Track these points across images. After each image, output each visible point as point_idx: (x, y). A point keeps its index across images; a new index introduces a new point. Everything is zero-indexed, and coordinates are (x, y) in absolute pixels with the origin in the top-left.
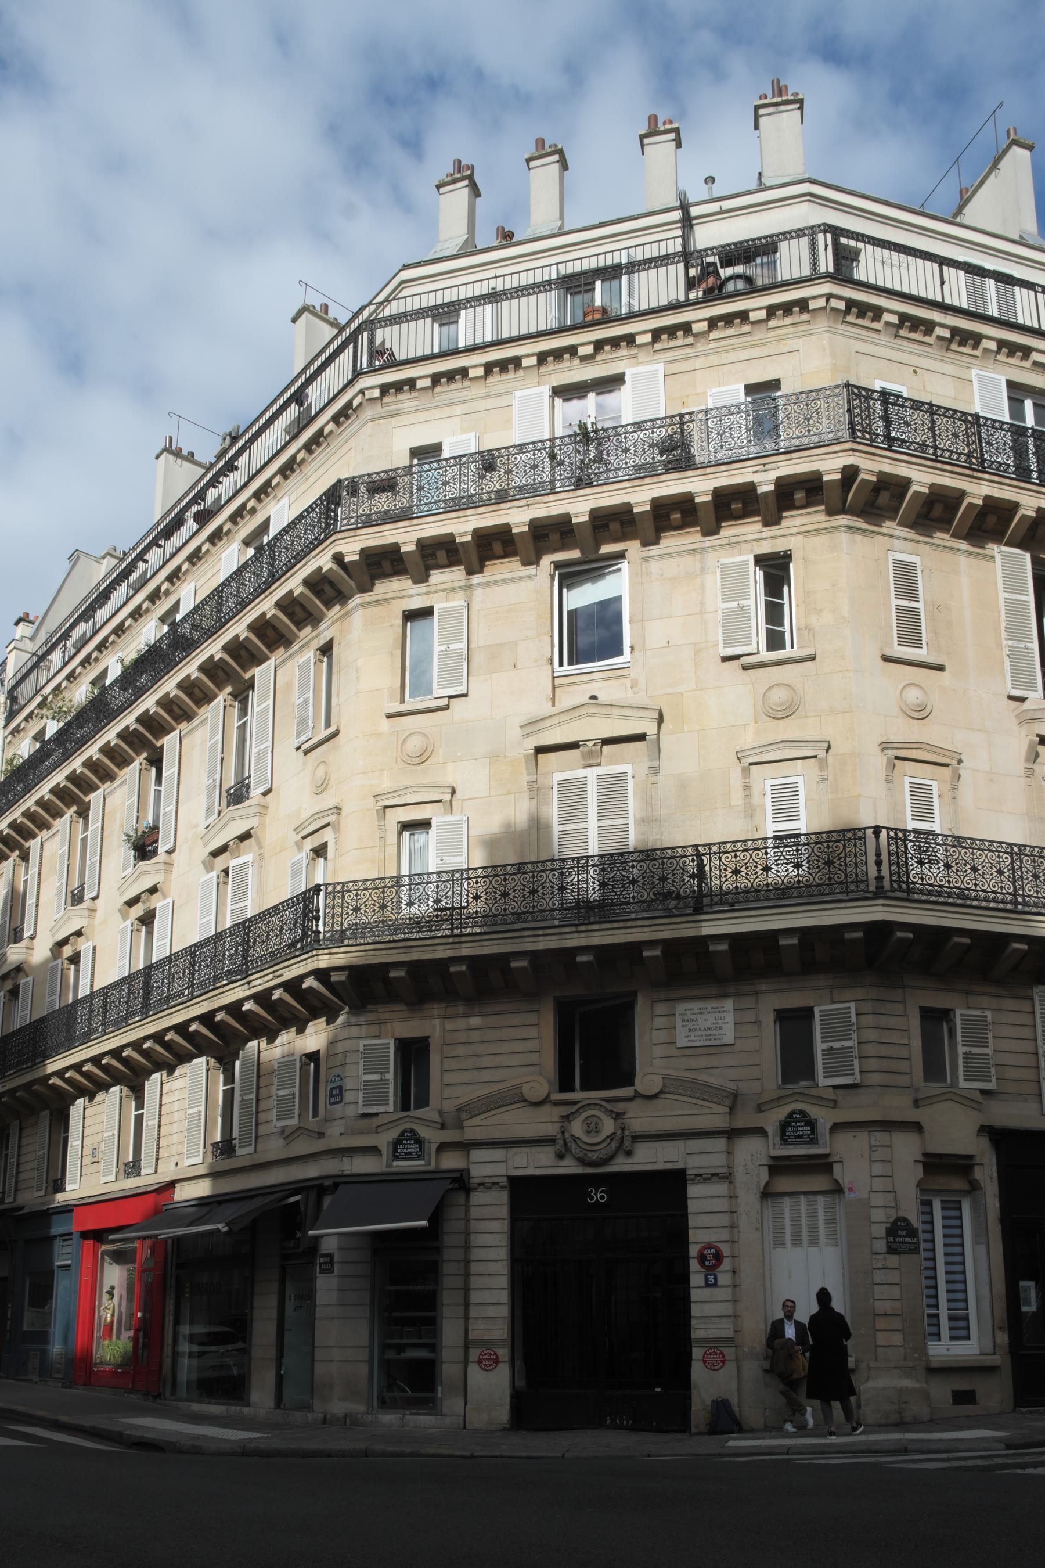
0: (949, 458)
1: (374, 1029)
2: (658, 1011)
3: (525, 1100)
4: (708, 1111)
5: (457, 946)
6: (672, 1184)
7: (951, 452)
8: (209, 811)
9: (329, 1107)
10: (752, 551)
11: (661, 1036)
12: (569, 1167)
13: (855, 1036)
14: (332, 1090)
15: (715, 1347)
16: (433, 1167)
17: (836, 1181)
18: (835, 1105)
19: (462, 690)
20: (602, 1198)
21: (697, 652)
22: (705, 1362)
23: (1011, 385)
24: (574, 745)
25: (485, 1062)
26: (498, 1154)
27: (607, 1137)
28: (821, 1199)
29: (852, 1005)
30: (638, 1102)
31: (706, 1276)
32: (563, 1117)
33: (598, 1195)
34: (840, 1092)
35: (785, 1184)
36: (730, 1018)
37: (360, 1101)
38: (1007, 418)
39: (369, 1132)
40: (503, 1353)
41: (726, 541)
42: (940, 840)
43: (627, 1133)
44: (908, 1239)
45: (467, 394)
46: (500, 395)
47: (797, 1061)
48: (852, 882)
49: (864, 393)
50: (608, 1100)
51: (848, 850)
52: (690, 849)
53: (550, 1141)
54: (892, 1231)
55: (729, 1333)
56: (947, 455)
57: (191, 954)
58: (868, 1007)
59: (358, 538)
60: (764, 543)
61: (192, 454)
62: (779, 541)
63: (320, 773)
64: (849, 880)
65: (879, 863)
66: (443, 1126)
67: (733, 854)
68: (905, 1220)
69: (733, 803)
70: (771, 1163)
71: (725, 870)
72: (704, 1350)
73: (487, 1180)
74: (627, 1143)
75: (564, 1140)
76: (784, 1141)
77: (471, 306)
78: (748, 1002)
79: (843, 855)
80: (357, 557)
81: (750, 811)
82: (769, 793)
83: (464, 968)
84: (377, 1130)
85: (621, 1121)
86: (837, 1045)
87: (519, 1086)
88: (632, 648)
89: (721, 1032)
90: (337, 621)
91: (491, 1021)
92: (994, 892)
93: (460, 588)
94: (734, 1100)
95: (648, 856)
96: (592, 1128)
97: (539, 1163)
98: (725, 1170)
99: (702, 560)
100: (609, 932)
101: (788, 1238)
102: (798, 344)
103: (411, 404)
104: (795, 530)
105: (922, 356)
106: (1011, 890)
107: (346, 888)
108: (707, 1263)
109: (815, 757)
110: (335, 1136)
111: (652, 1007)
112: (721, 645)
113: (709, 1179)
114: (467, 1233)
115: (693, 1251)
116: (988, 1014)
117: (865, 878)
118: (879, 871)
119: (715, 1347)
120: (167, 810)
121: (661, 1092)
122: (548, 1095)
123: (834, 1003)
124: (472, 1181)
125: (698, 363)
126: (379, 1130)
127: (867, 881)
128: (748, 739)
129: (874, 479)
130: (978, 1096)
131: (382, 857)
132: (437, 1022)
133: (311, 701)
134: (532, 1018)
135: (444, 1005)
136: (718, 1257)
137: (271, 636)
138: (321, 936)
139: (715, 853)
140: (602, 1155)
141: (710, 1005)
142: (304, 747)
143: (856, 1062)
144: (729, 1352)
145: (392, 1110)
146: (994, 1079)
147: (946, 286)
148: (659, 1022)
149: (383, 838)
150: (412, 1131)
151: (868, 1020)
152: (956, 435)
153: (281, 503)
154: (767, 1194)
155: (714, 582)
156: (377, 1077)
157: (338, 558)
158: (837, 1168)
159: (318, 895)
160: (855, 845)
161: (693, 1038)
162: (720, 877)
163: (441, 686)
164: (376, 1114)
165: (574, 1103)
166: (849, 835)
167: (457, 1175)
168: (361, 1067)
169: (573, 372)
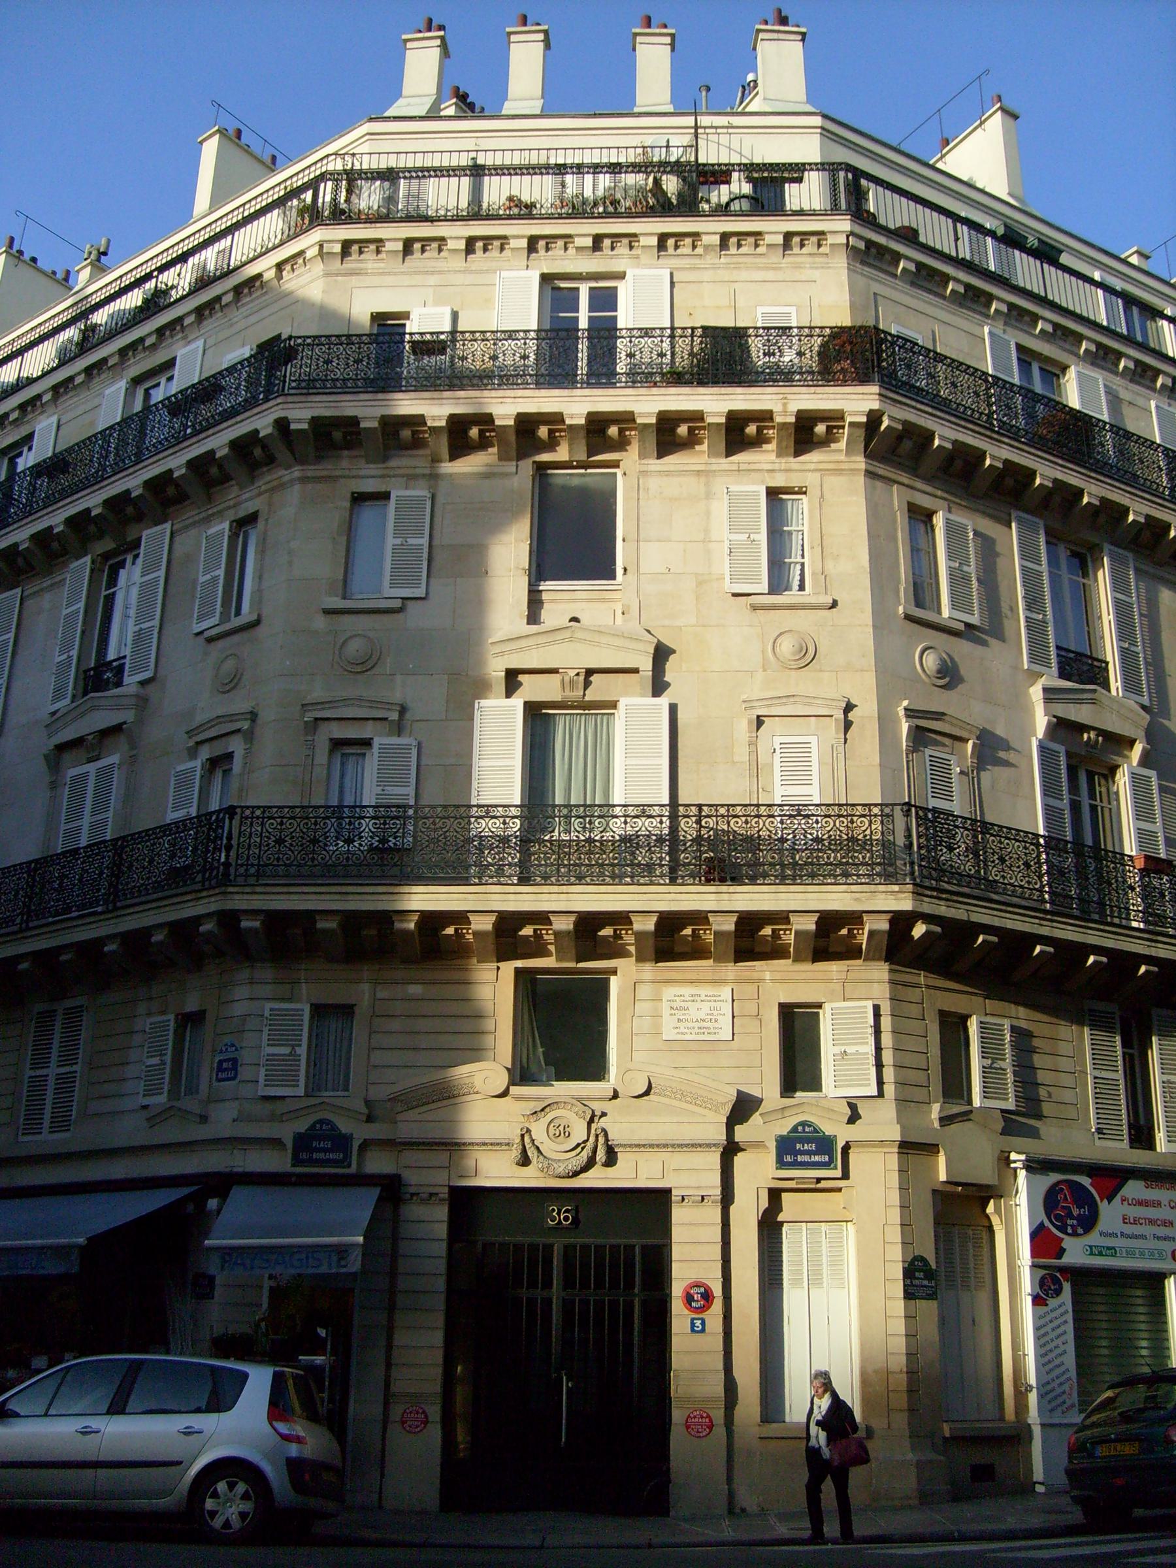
0: (963, 413)
7: (973, 411)
8: (58, 694)
10: (763, 482)
16: (353, 1169)
19: (420, 592)
20: (566, 1219)
21: (700, 584)
22: (688, 1427)
23: (1020, 348)
24: (554, 671)
27: (578, 1145)
31: (693, 1320)
38: (1016, 381)
39: (272, 1118)
41: (735, 467)
42: (959, 822)
44: (926, 1283)
45: (441, 265)
46: (481, 272)
49: (889, 338)
51: (873, 827)
52: (693, 808)
54: (908, 1273)
56: (969, 413)
57: (28, 872)
59: (309, 405)
60: (778, 475)
61: (34, 260)
62: (793, 475)
63: (230, 665)
66: (370, 1119)
68: (922, 1259)
73: (422, 1190)
77: (456, 175)
79: (868, 832)
80: (305, 426)
81: (756, 769)
84: (281, 1118)
88: (625, 570)
89: (716, 1025)
90: (266, 491)
92: (1021, 887)
93: (424, 475)
95: (644, 811)
99: (707, 484)
102: (816, 274)
103: (376, 265)
104: (812, 466)
105: (935, 306)
106: (1037, 887)
107: (267, 814)
108: (694, 1304)
110: (224, 1120)
112: (727, 580)
115: (677, 1290)
124: (403, 1189)
125: (707, 276)
128: (756, 689)
129: (900, 427)
132: (366, 987)
133: (221, 581)
135: (377, 967)
136: (707, 1296)
137: (165, 497)
138: (232, 870)
139: (723, 816)
142: (207, 634)
145: (301, 1091)
147: (960, 243)
150: (329, 1122)
152: (977, 394)
153: (193, 346)
155: (720, 508)
156: (286, 1050)
157: (282, 425)
159: (231, 819)
161: (682, 1030)
163: (393, 585)
164: (283, 1098)
168: (265, 1037)
169: (566, 262)
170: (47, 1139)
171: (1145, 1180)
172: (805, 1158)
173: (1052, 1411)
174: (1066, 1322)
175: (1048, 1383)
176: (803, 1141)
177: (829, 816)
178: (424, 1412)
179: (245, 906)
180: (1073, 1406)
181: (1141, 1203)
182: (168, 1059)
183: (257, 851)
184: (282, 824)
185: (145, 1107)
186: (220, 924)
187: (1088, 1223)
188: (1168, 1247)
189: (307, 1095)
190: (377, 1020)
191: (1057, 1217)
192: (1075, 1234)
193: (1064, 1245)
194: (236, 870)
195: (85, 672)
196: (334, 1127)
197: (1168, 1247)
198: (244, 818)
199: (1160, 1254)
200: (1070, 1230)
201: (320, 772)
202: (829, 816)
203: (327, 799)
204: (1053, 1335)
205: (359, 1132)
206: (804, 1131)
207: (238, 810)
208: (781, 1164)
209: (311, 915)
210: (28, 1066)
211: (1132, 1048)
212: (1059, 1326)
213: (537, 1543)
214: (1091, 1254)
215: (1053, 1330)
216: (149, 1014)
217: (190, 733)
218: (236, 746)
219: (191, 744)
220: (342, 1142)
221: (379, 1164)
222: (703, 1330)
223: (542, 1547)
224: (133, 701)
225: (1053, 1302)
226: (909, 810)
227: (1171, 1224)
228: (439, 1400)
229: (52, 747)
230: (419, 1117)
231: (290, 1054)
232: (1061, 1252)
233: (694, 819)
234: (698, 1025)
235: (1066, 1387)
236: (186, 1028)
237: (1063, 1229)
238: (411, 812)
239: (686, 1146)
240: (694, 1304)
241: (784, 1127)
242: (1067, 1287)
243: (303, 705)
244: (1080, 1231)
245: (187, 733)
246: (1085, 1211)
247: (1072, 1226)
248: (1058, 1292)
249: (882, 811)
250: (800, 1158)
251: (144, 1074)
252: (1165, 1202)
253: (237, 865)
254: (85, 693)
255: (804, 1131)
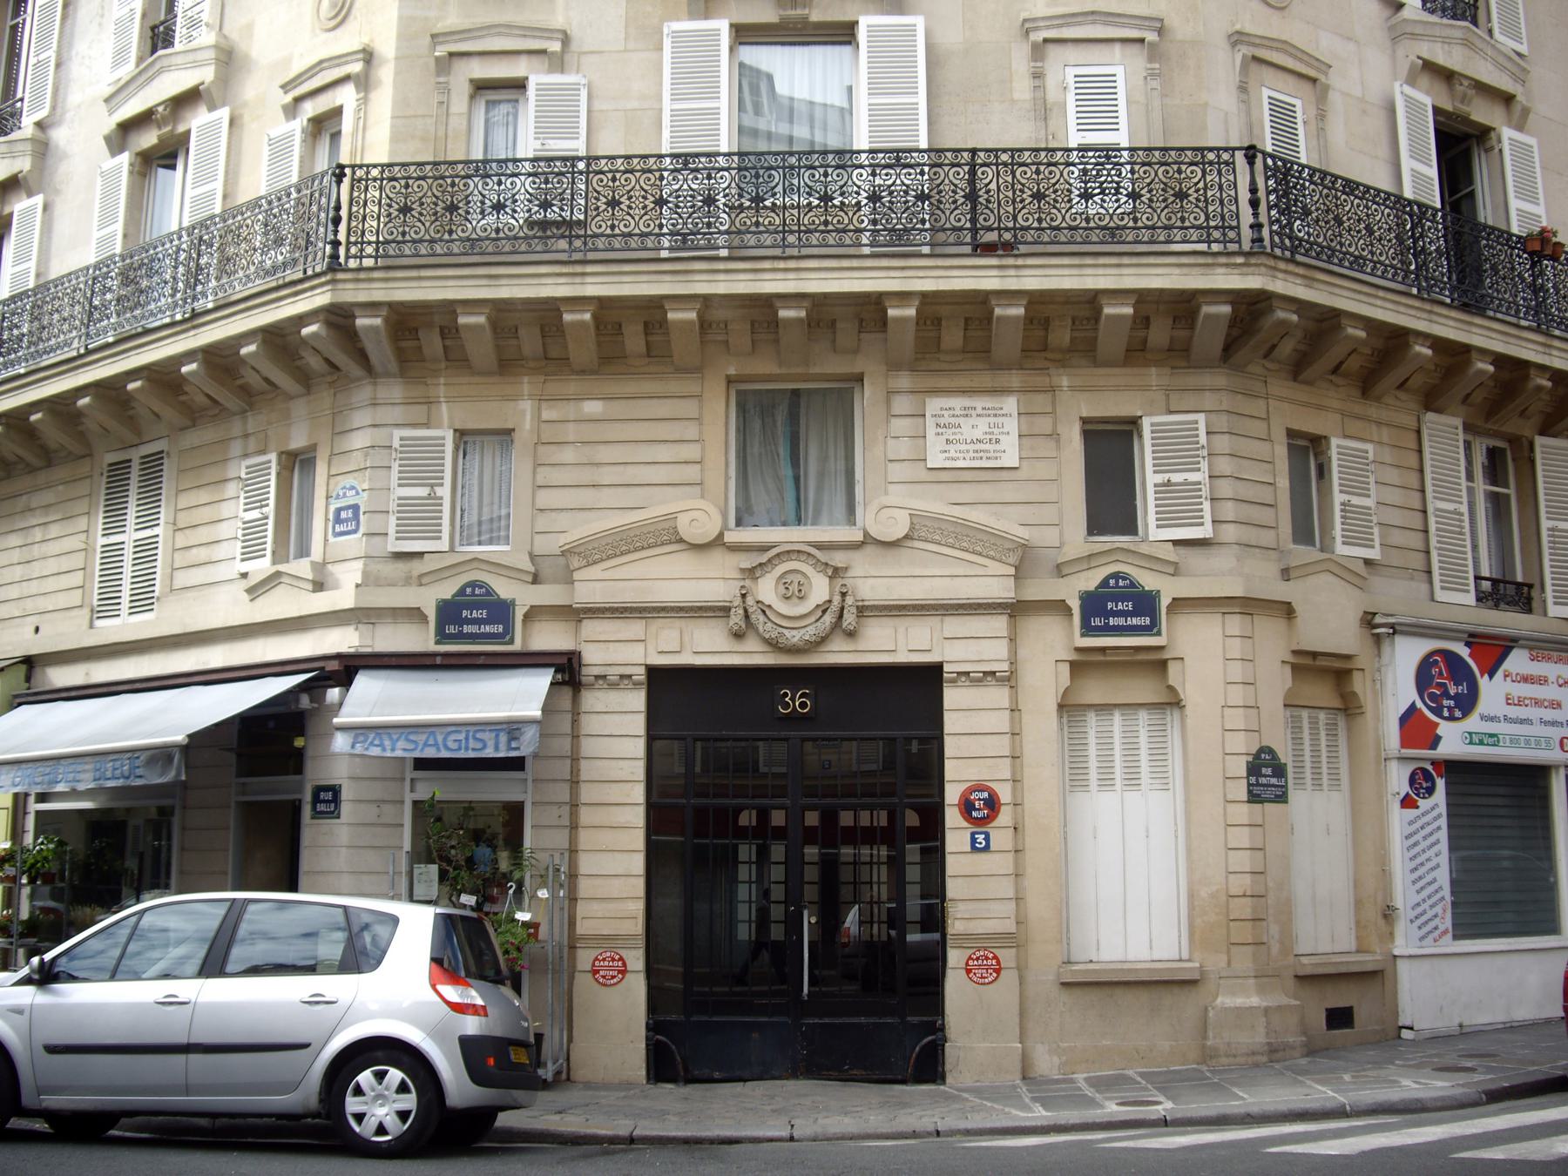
1: (419, 412)
2: (896, 410)
3: (681, 541)
4: (981, 571)
5: (578, 280)
6: (922, 684)
8: (119, 58)
9: (332, 539)
11: (902, 448)
12: (752, 654)
13: (1204, 465)
14: (339, 511)
15: (985, 949)
16: (517, 646)
17: (1171, 689)
18: (1176, 570)
20: (803, 705)
22: (968, 971)
25: (607, 475)
26: (635, 628)
28: (1143, 715)
29: (1201, 417)
30: (869, 549)
31: (973, 834)
32: (743, 570)
33: (796, 701)
34: (1182, 550)
35: (1095, 690)
36: (1012, 425)
37: (392, 530)
40: (636, 960)
43: (849, 600)
44: (1274, 781)
47: (1112, 504)
48: (1216, 228)
50: (820, 546)
51: (1209, 178)
52: (965, 154)
53: (724, 611)
54: (1253, 769)
55: (1010, 926)
58: (1222, 422)
64: (1212, 223)
65: (1254, 204)
66: (536, 580)
67: (1034, 168)
68: (1270, 751)
69: (1016, 96)
70: (1074, 657)
71: (1022, 191)
72: (971, 951)
74: (849, 619)
75: (746, 611)
76: (1088, 630)
78: (1041, 401)
79: (1201, 185)
81: (1044, 111)
82: (1072, 85)
83: (587, 316)
84: (421, 580)
85: (841, 582)
86: (1177, 478)
87: (672, 517)
91: (618, 409)
94: (1024, 560)
95: (898, 159)
96: (793, 590)
97: (707, 647)
98: (1005, 666)
100: (835, 275)
101: (1093, 775)
108: (974, 814)
109: (1142, 41)
111: (888, 403)
113: (979, 680)
114: (575, 758)
115: (952, 794)
116: (1369, 447)
117: (1234, 223)
118: (1256, 215)
119: (985, 949)
120: (41, 57)
121: (906, 537)
122: (721, 535)
123: (1171, 412)
124: (585, 671)
126: (424, 581)
127: (1238, 227)
130: (1360, 568)
131: (441, 133)
132: (527, 406)
134: (689, 408)
135: (542, 378)
136: (993, 804)
139: (1005, 164)
140: (809, 633)
141: (980, 403)
143: (1207, 506)
144: (1007, 956)
145: (444, 545)
146: (1377, 543)
148: (899, 425)
149: (444, 105)
151: (1223, 443)
154: (1068, 708)
156: (422, 492)
158: (1173, 668)
159: (339, 182)
160: (1219, 172)
161: (952, 454)
162: (1014, 201)
164: (421, 554)
165: (764, 548)
166: (1211, 156)
167: (564, 660)
168: (395, 474)
170: (125, 625)
171: (1531, 649)
172: (1120, 621)
173: (1422, 938)
174: (1439, 828)
175: (1418, 904)
176: (1117, 598)
177: (1149, 164)
178: (621, 959)
179: (362, 297)
180: (1445, 932)
181: (1526, 679)
182: (270, 510)
183: (375, 224)
184: (407, 186)
185: (244, 575)
186: (329, 324)
187: (1467, 703)
188: (1556, 733)
189: (452, 550)
190: (541, 449)
191: (1433, 697)
192: (1452, 718)
193: (1439, 731)
194: (348, 250)
195: (153, 28)
196: (490, 592)
197: (1556, 733)
198: (355, 181)
199: (1548, 743)
200: (1446, 714)
201: (457, 123)
202: (1149, 164)
203: (468, 152)
204: (1424, 844)
205: (523, 596)
206: (1117, 585)
207: (347, 171)
208: (1088, 630)
209: (450, 308)
210: (100, 532)
211: (1506, 486)
212: (1431, 834)
213: (785, 1133)
214: (1471, 743)
215: (1425, 838)
216: (246, 456)
217: (285, 87)
218: (346, 97)
219: (289, 98)
220: (501, 611)
221: (550, 638)
222: (987, 848)
223: (792, 1139)
224: (211, 54)
225: (1424, 804)
226: (1254, 156)
227: (1559, 705)
228: (641, 943)
229: (113, 126)
230: (607, 575)
231: (429, 497)
232: (1435, 741)
233: (966, 168)
234: (971, 447)
235: (1438, 909)
236: (292, 471)
237: (1437, 712)
238: (581, 165)
239: (970, 606)
240: (974, 814)
241: (1090, 581)
242: (1440, 784)
243: (433, 36)
244: (1458, 714)
245: (282, 87)
246: (1463, 689)
247: (1449, 708)
248: (1430, 791)
249: (1219, 156)
250: (1112, 621)
251: (240, 532)
252: (1552, 678)
253: (348, 242)
254: (154, 51)
255: (1117, 585)
